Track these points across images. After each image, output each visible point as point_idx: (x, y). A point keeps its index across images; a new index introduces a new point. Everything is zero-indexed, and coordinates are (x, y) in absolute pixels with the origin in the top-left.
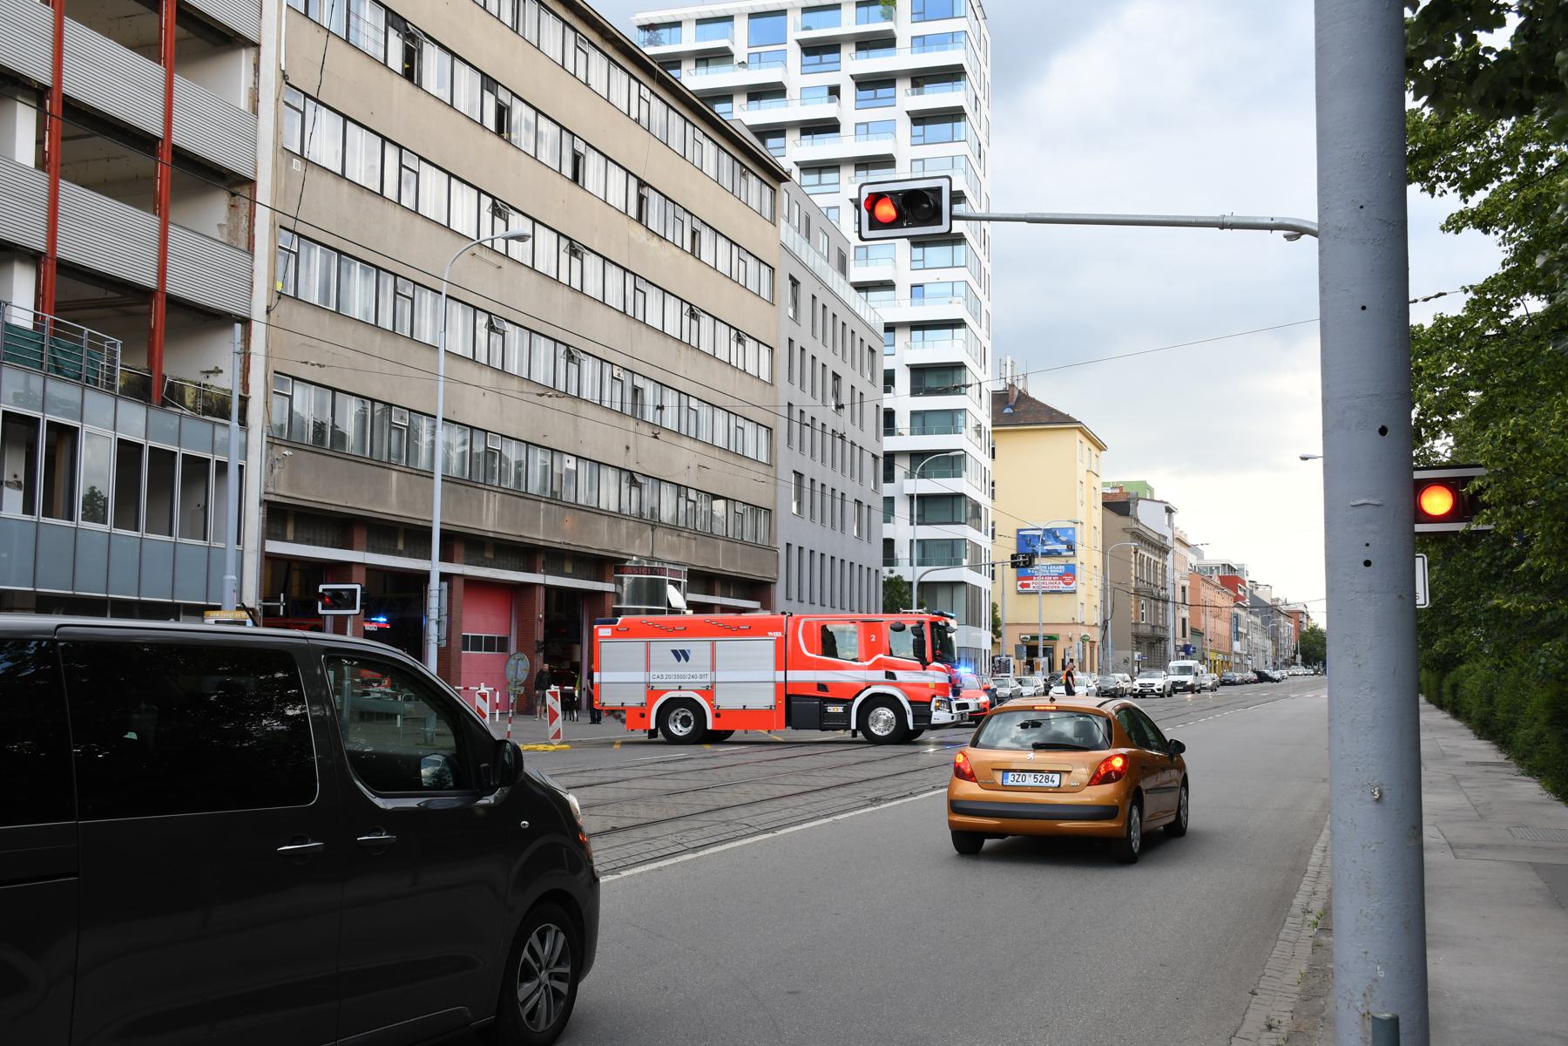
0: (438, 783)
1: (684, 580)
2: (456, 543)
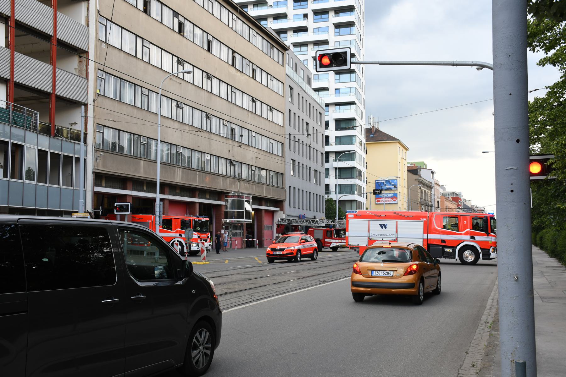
0: (161, 276)
2: (166, 187)
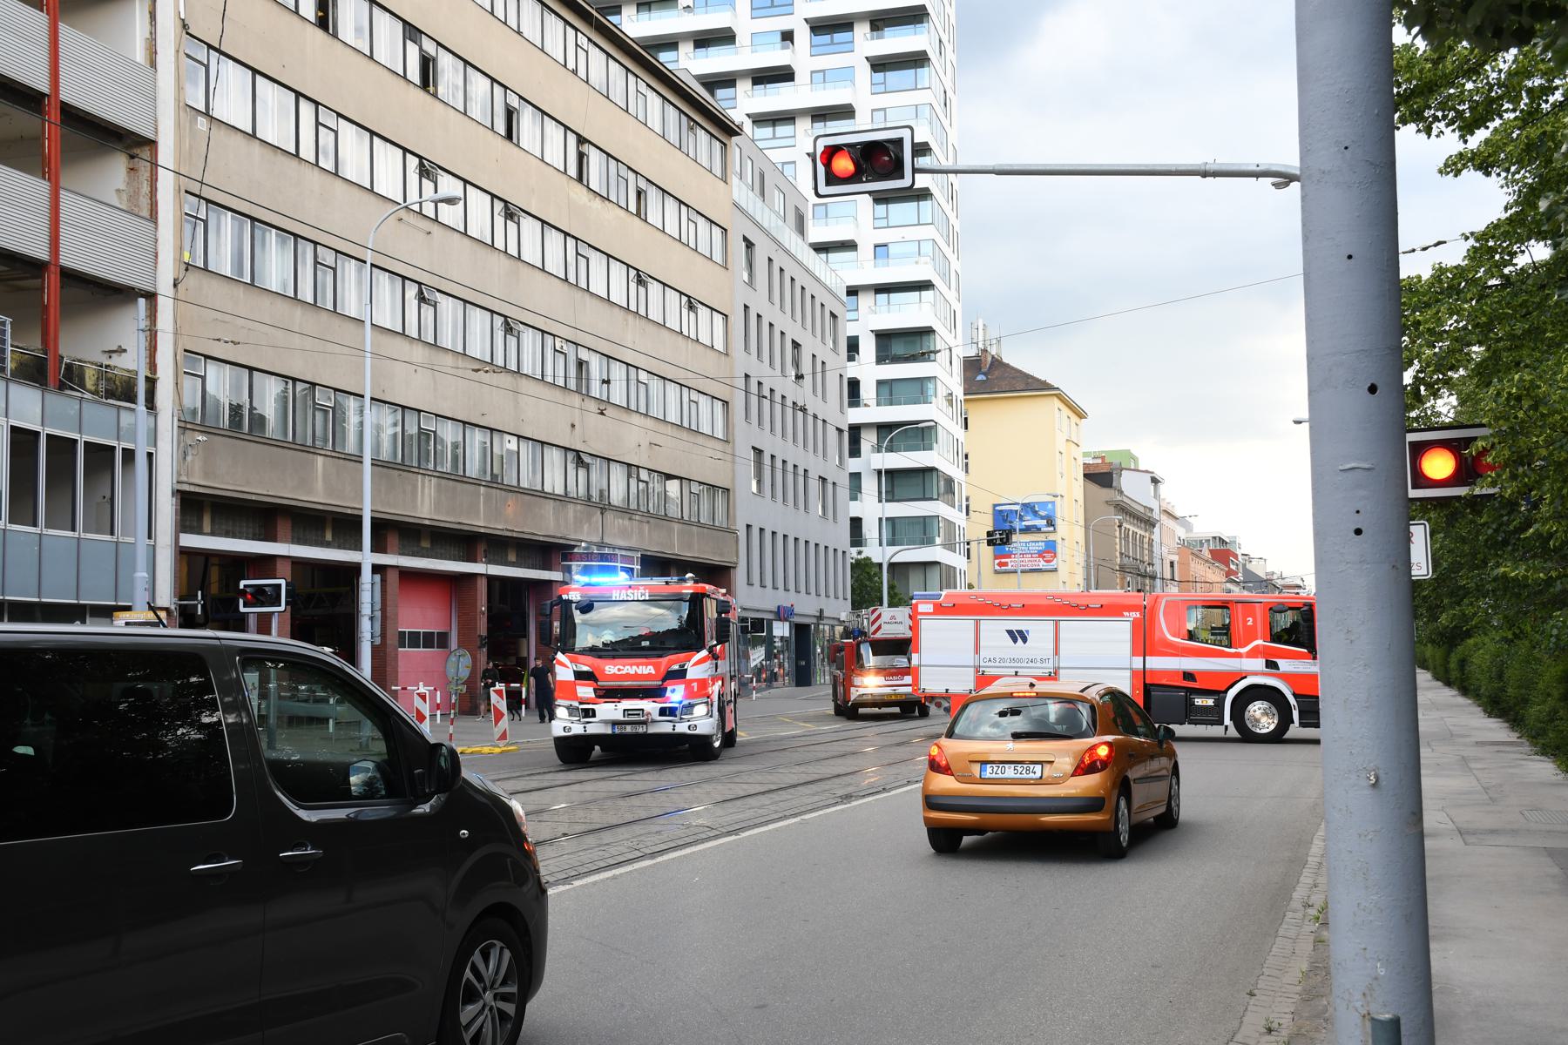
0: (369, 792)
2: (388, 531)
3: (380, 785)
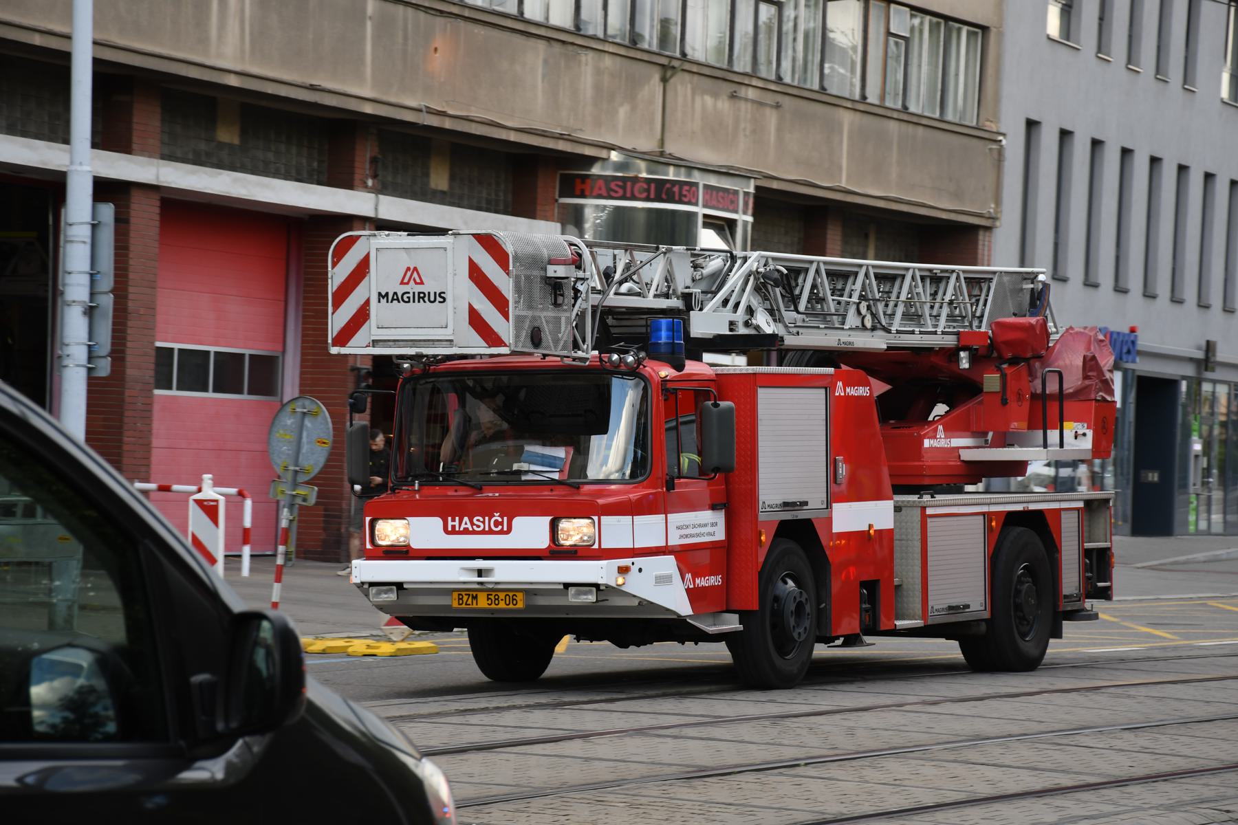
0: (78, 720)
1: (745, 218)
2: (137, 98)
3: (105, 709)
